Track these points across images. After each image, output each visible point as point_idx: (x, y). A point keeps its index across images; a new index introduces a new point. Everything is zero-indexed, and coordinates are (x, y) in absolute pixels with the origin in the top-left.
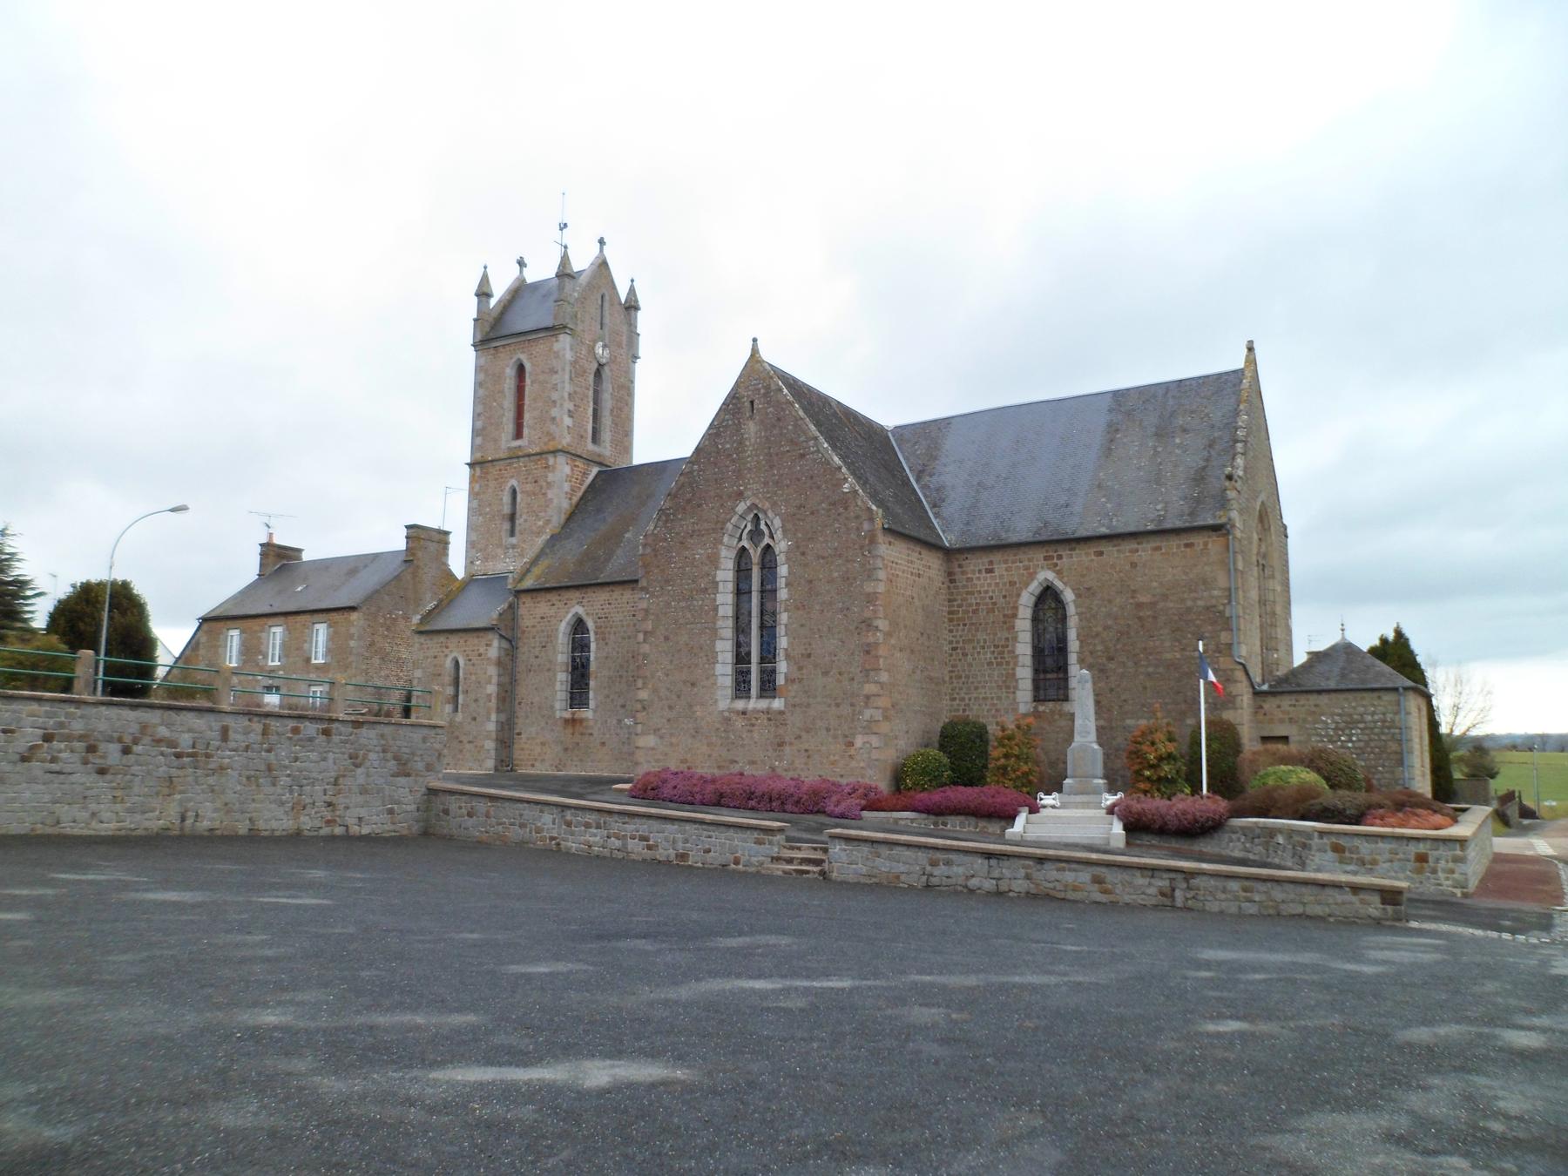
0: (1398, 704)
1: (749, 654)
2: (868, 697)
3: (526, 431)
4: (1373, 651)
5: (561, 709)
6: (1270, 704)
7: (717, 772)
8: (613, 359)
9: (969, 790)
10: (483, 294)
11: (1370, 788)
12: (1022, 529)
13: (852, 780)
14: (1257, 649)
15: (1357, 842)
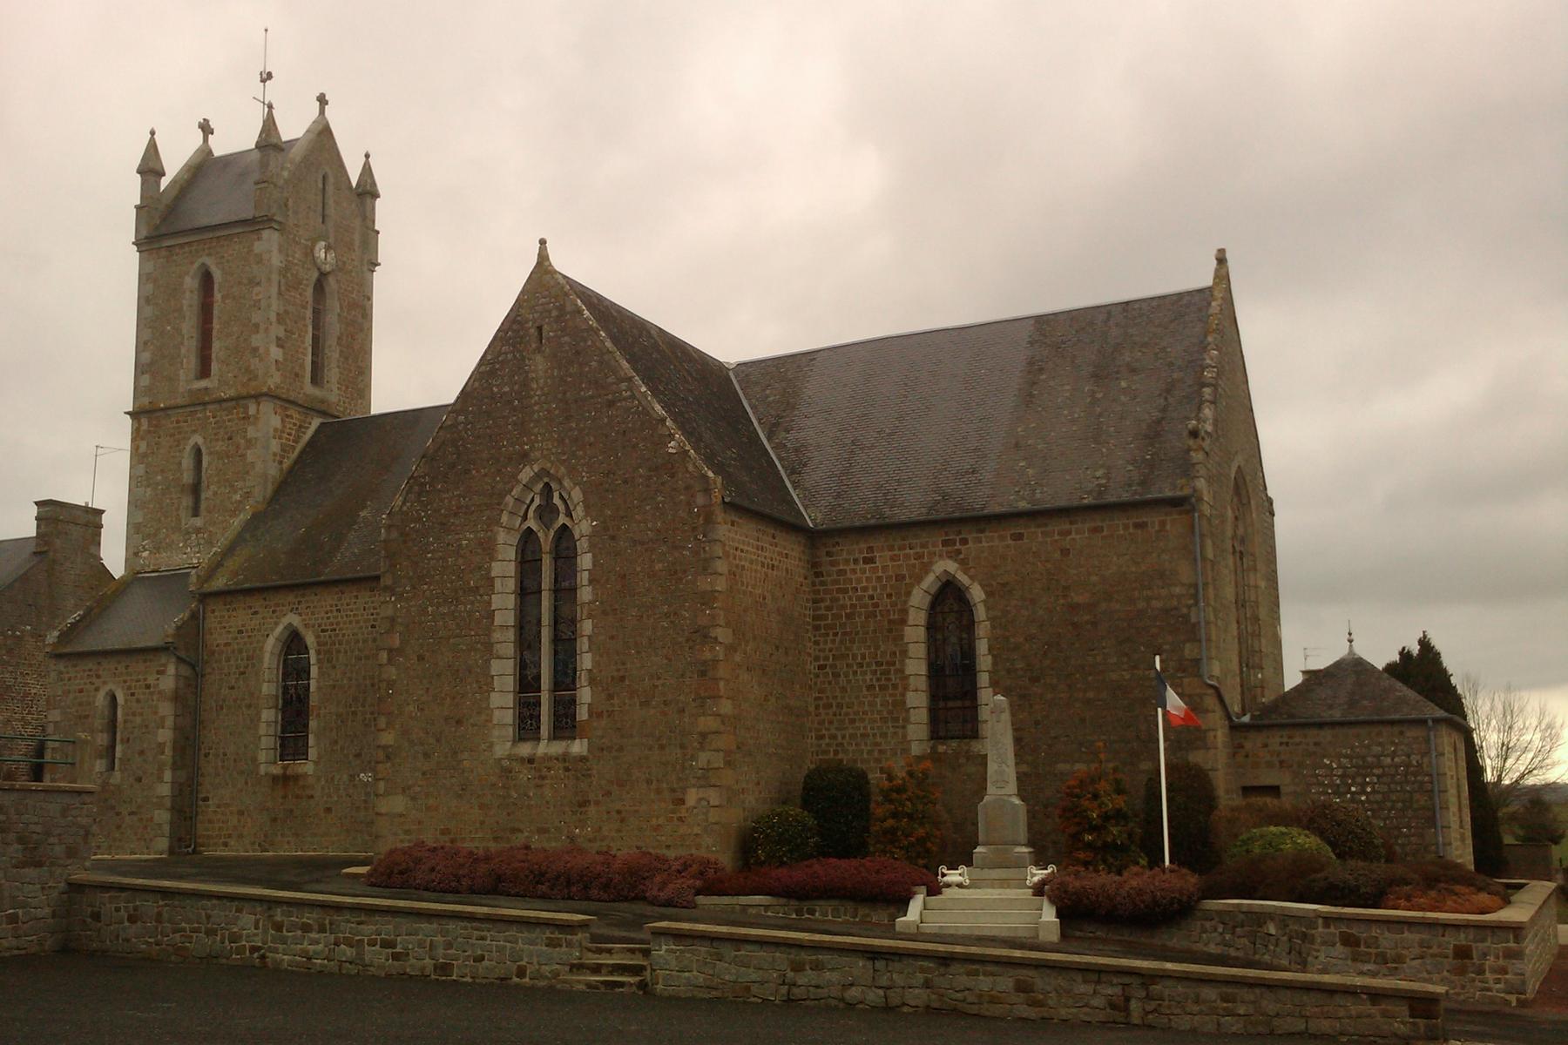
0: (1427, 740)
1: (538, 678)
2: (704, 735)
3: (215, 367)
4: (1391, 669)
5: (267, 762)
6: (1253, 742)
7: (493, 846)
8: (340, 268)
9: (844, 863)
10: (150, 168)
11: (1391, 858)
12: (913, 503)
13: (683, 852)
14: (1235, 666)
15: (1375, 931)
